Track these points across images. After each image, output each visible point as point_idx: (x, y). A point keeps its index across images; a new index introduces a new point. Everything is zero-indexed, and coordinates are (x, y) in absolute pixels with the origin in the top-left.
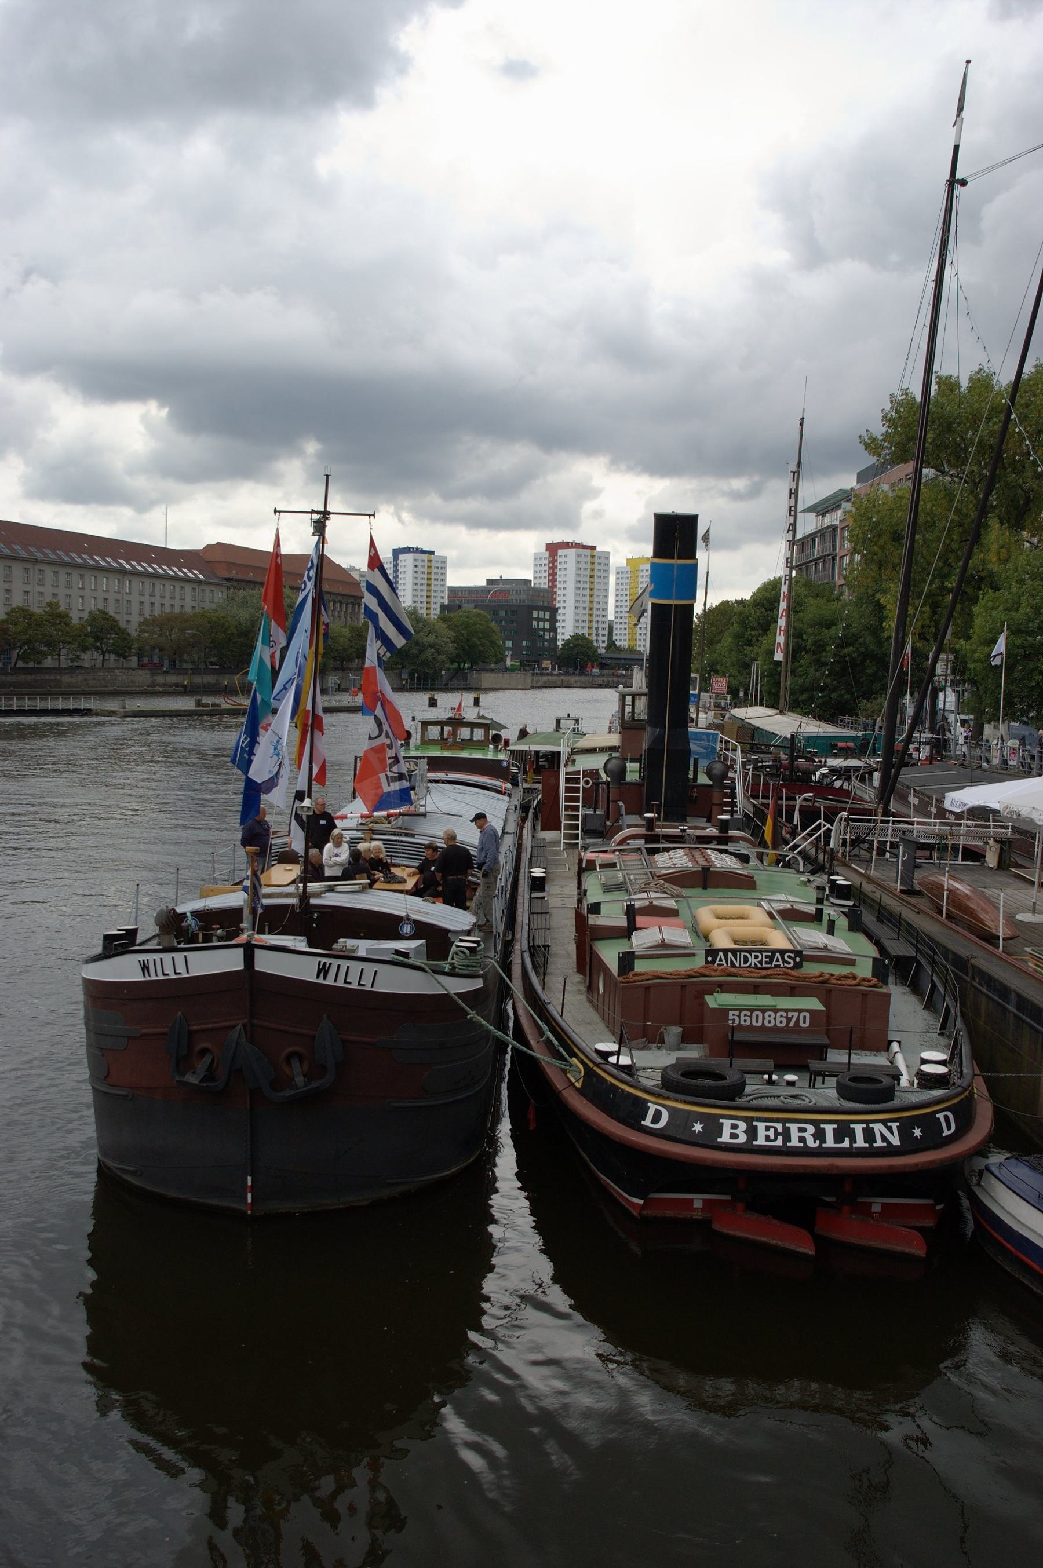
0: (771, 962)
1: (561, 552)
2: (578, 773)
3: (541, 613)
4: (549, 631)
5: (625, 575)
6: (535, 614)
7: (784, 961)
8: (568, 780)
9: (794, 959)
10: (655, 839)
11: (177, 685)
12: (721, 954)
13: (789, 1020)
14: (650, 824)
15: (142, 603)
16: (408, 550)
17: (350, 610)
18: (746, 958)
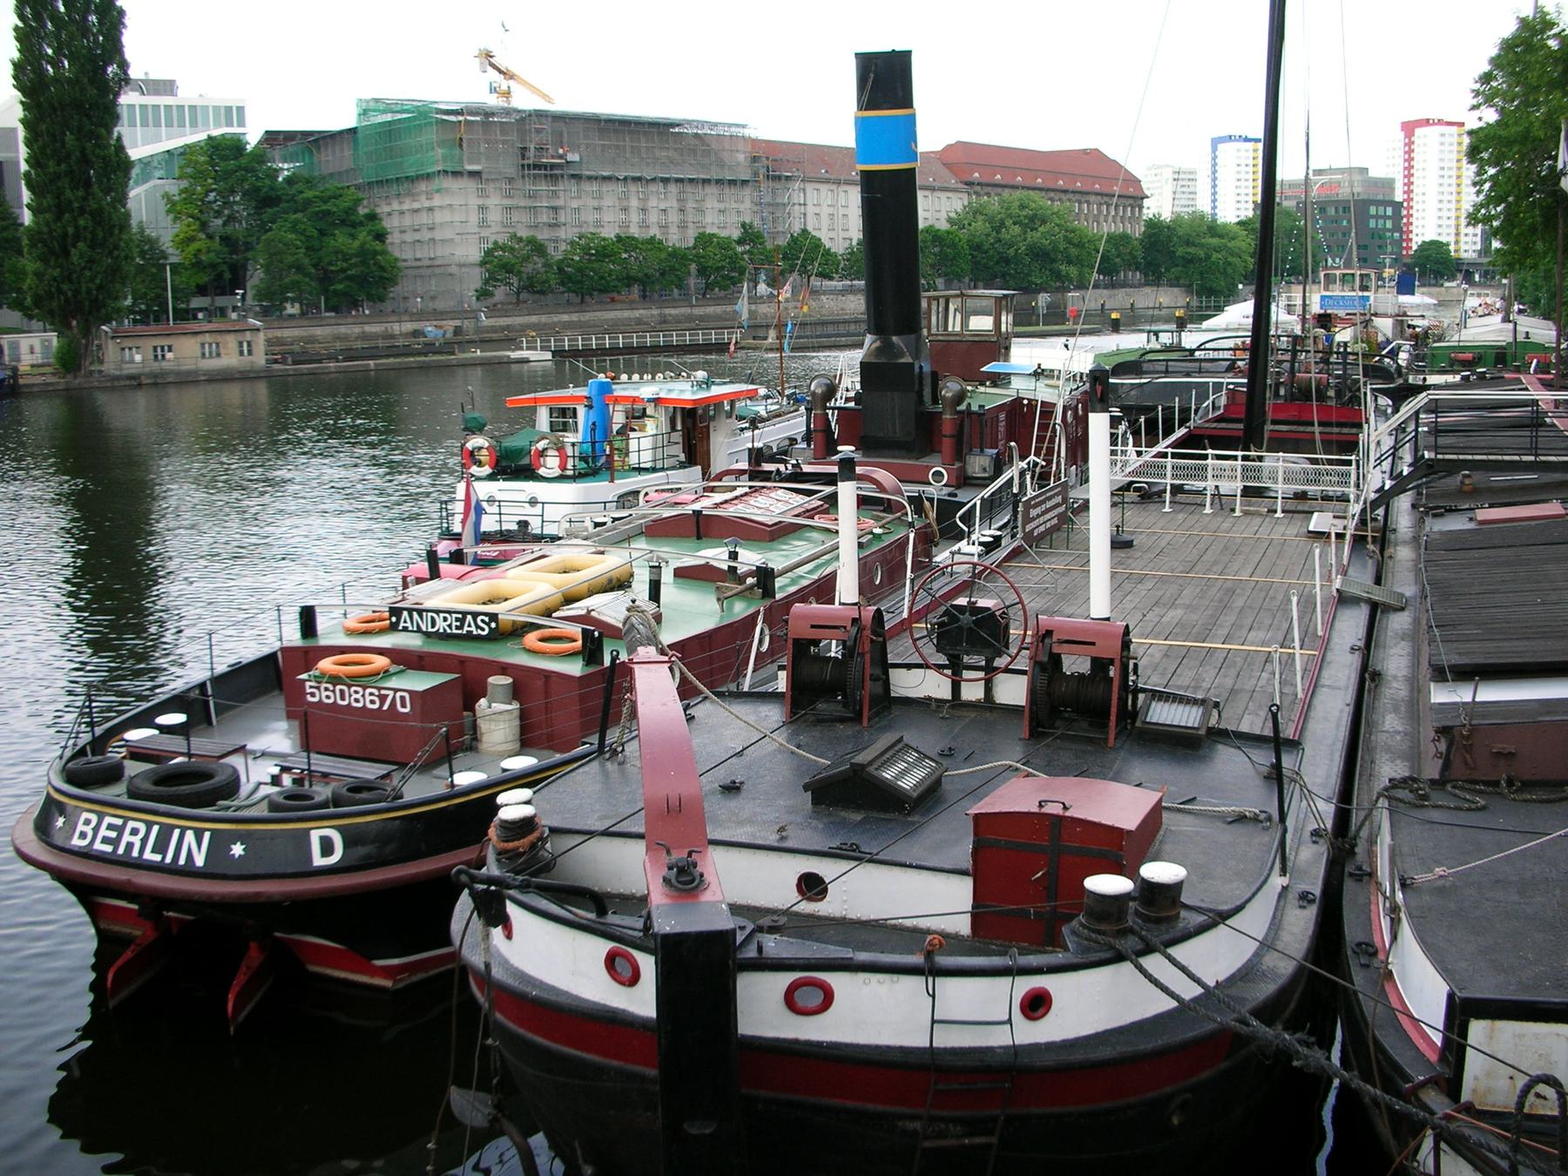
0: (461, 627)
1: (1418, 131)
3: (1381, 209)
4: (1392, 231)
6: (1373, 210)
7: (478, 627)
9: (488, 624)
13: (383, 698)
18: (433, 620)
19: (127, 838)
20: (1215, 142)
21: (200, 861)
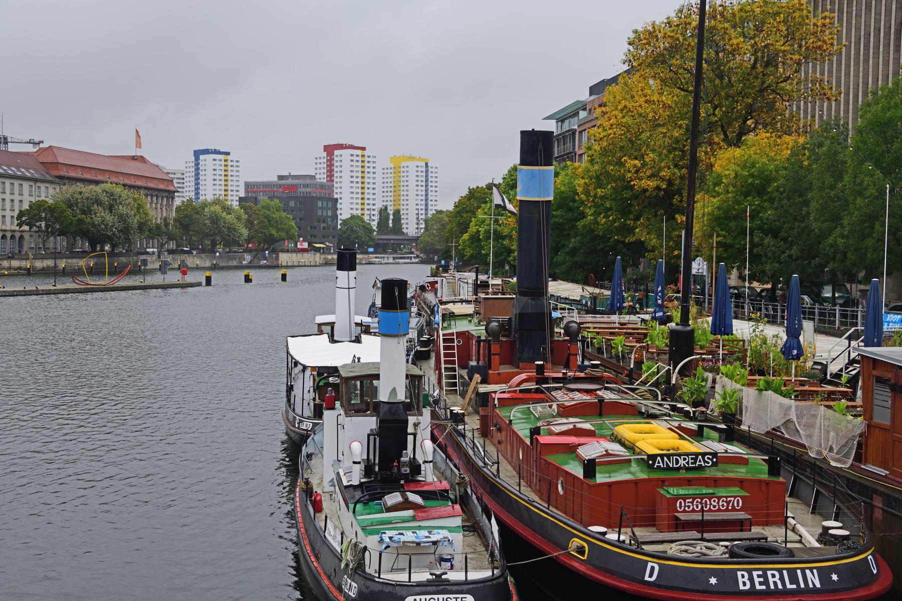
0: (695, 463)
1: (336, 152)
2: (452, 334)
5: (389, 171)
6: (320, 204)
7: (705, 461)
8: (445, 341)
9: (712, 460)
10: (546, 380)
11: (20, 268)
12: (659, 458)
13: (728, 503)
14: (540, 369)
15: (3, 200)
16: (207, 152)
17: (165, 202)
19: (771, 580)
20: (197, 154)
21: (818, 585)
